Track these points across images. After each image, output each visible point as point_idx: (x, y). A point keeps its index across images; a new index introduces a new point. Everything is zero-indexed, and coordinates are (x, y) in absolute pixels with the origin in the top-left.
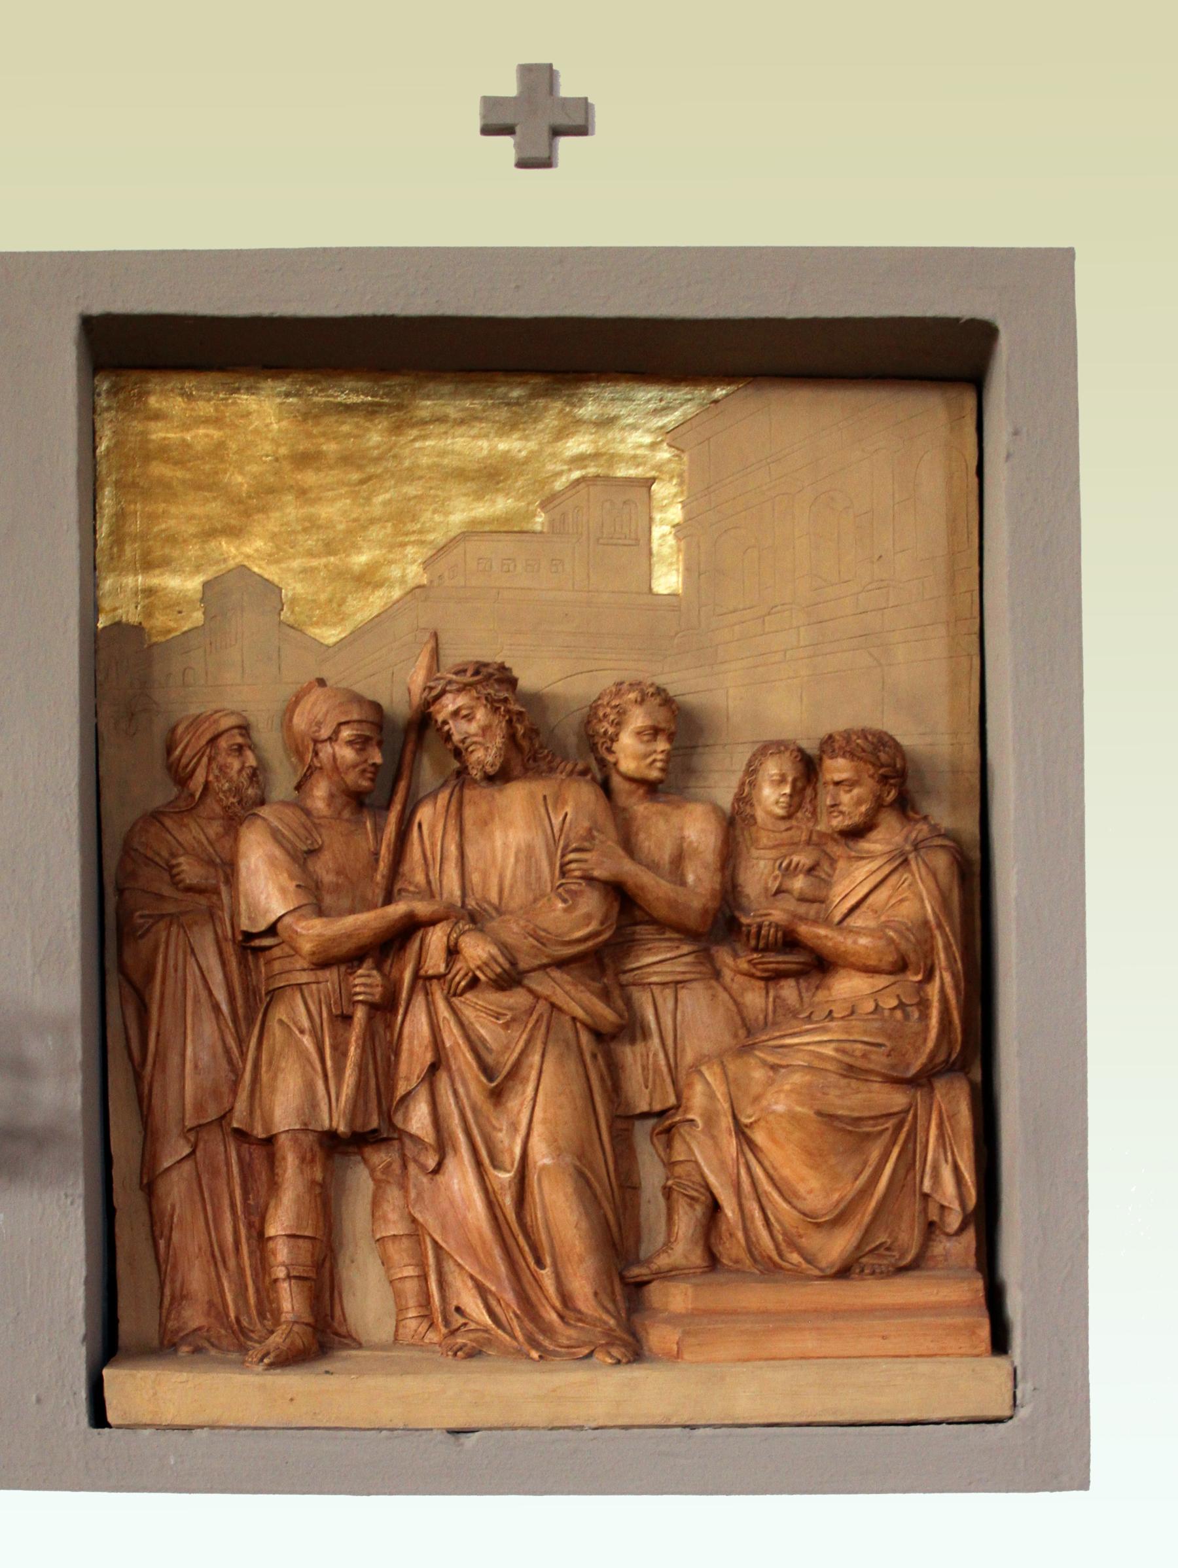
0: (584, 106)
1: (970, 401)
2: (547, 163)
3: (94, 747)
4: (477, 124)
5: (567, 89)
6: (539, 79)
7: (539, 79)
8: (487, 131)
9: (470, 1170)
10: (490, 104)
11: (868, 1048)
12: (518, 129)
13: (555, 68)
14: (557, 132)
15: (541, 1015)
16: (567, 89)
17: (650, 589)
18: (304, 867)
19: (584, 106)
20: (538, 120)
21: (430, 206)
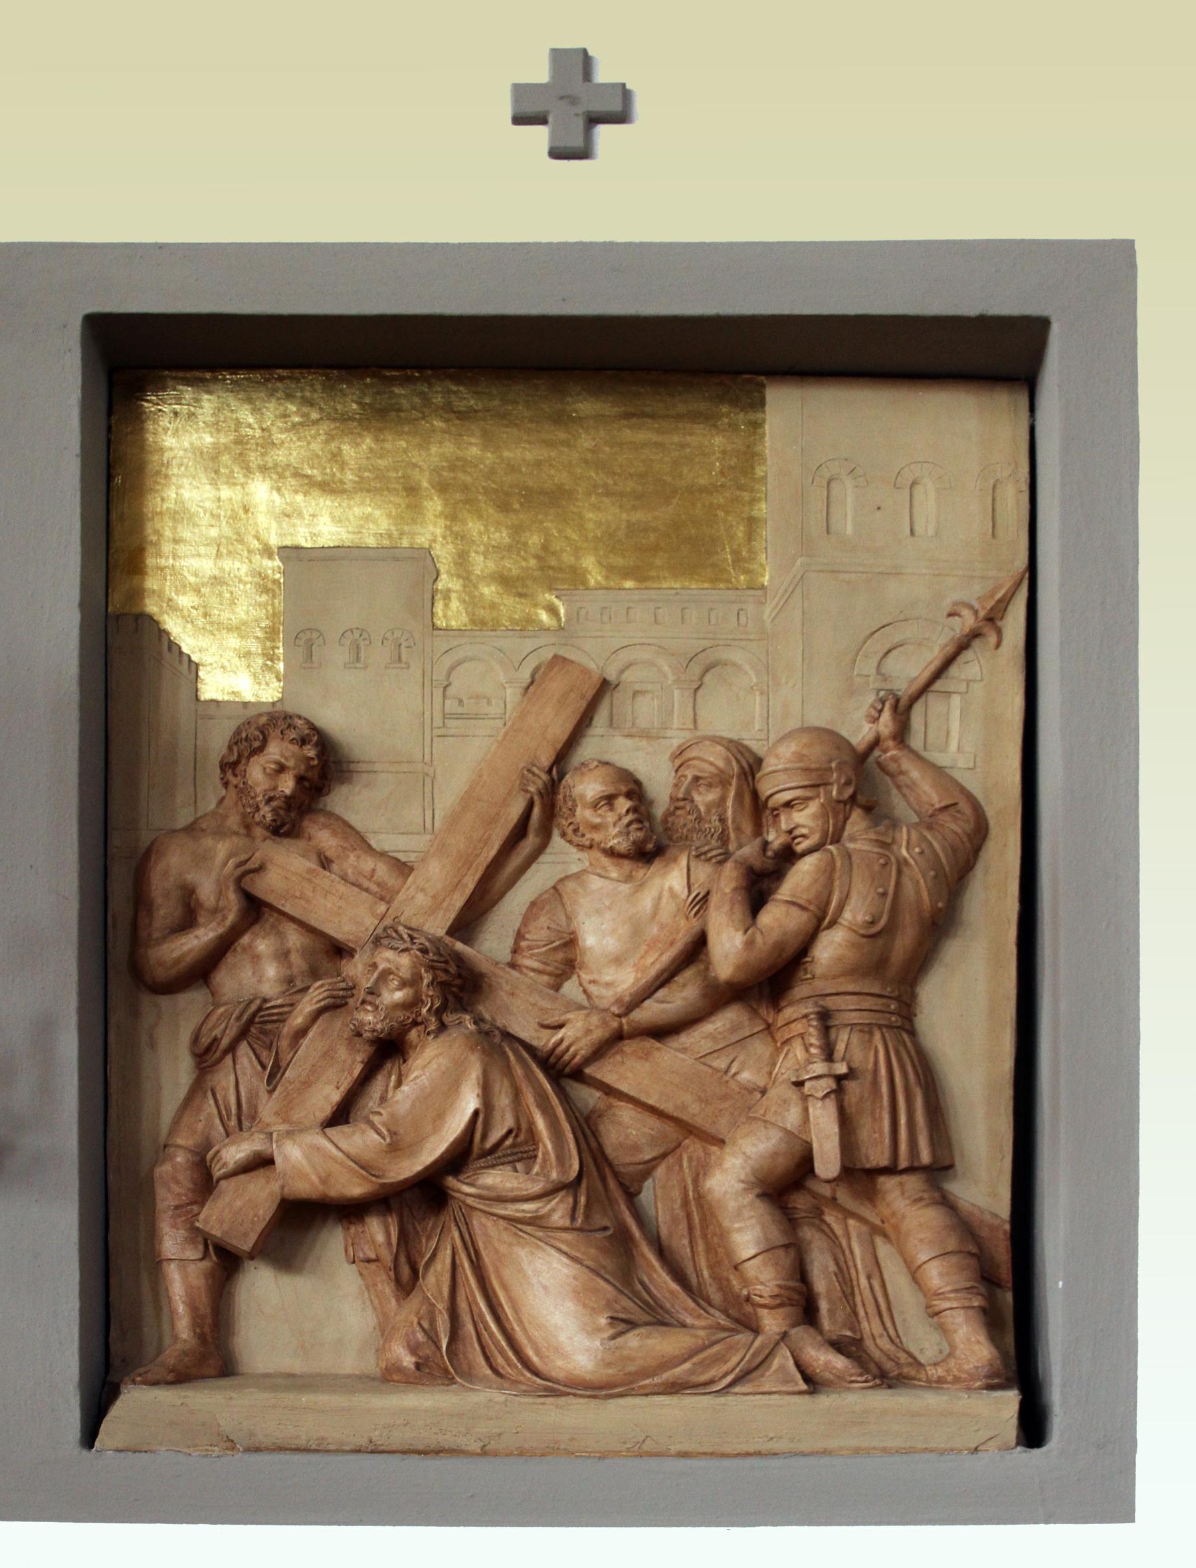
0: (625, 94)
1: (1024, 400)
2: (584, 153)
3: (101, 1117)
6: (576, 64)
8: (518, 120)
9: (660, 1270)
10: (520, 91)
11: (869, 1077)
12: (550, 119)
13: (628, 87)
14: (594, 120)
15: (229, 1119)
16: (604, 74)
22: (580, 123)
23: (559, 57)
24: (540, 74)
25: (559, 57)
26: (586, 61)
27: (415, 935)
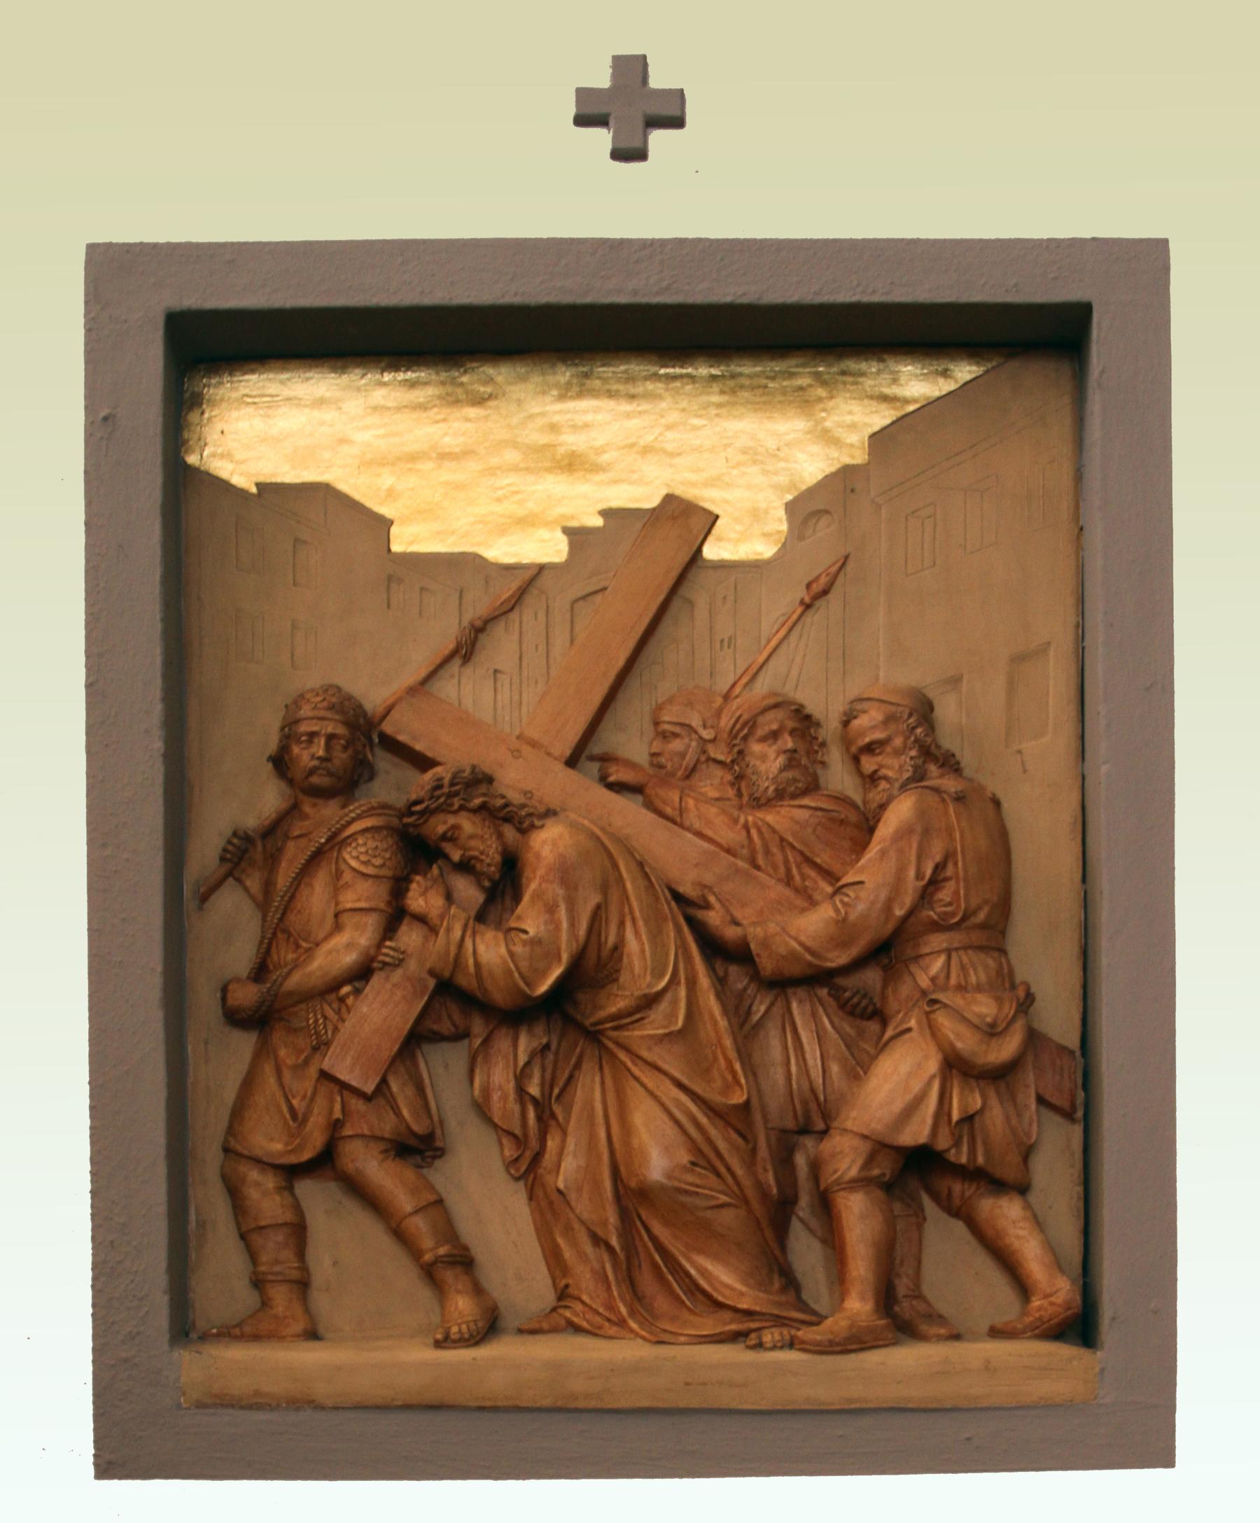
4: (572, 111)
5: (657, 81)
6: (631, 69)
7: (631, 69)
8: (582, 120)
10: (583, 95)
12: (612, 122)
13: (648, 60)
14: (655, 122)
16: (657, 81)
20: (632, 112)
22: (640, 123)
23: (620, 63)
24: (602, 79)
25: (620, 63)
26: (641, 63)
27: (551, 1057)
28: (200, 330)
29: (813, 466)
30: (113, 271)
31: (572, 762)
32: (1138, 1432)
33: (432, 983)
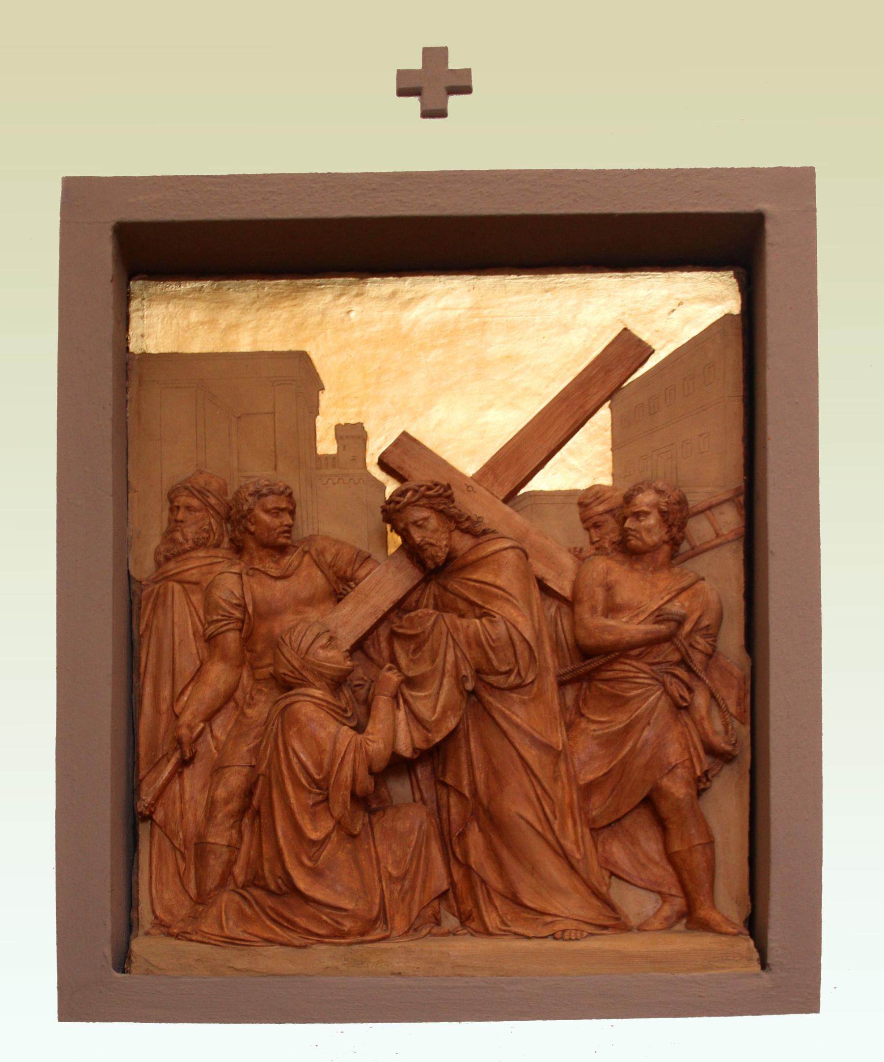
5: (454, 63)
6: (435, 56)
7: (435, 56)
10: (402, 75)
16: (454, 63)
17: (128, 348)
18: (200, 546)
19: (467, 73)
21: (373, 142)
24: (416, 64)
25: (442, 114)
28: (148, 241)
29: (477, 829)
30: (80, 196)
31: (506, 501)
32: (791, 986)
33: (348, 654)
